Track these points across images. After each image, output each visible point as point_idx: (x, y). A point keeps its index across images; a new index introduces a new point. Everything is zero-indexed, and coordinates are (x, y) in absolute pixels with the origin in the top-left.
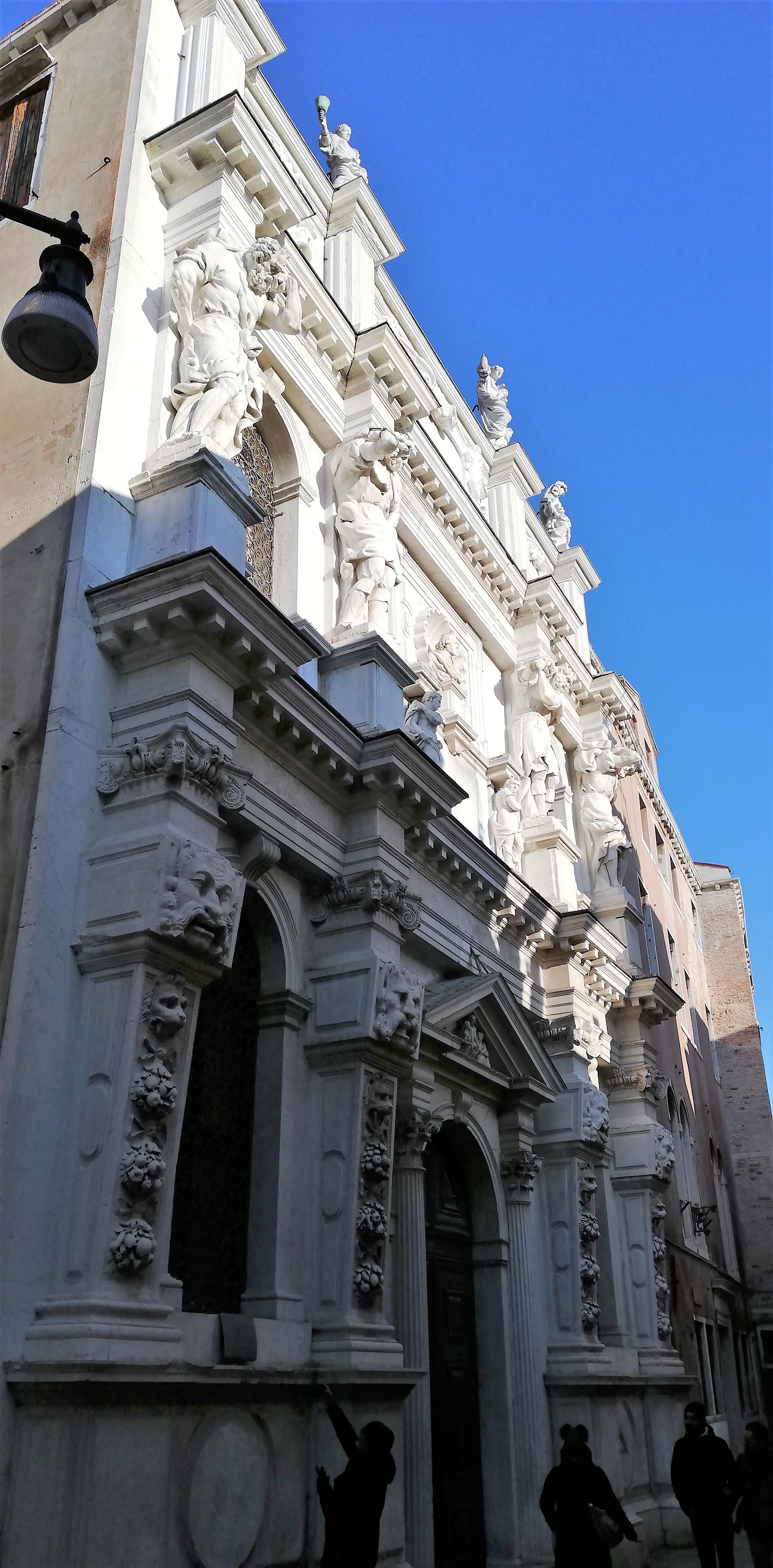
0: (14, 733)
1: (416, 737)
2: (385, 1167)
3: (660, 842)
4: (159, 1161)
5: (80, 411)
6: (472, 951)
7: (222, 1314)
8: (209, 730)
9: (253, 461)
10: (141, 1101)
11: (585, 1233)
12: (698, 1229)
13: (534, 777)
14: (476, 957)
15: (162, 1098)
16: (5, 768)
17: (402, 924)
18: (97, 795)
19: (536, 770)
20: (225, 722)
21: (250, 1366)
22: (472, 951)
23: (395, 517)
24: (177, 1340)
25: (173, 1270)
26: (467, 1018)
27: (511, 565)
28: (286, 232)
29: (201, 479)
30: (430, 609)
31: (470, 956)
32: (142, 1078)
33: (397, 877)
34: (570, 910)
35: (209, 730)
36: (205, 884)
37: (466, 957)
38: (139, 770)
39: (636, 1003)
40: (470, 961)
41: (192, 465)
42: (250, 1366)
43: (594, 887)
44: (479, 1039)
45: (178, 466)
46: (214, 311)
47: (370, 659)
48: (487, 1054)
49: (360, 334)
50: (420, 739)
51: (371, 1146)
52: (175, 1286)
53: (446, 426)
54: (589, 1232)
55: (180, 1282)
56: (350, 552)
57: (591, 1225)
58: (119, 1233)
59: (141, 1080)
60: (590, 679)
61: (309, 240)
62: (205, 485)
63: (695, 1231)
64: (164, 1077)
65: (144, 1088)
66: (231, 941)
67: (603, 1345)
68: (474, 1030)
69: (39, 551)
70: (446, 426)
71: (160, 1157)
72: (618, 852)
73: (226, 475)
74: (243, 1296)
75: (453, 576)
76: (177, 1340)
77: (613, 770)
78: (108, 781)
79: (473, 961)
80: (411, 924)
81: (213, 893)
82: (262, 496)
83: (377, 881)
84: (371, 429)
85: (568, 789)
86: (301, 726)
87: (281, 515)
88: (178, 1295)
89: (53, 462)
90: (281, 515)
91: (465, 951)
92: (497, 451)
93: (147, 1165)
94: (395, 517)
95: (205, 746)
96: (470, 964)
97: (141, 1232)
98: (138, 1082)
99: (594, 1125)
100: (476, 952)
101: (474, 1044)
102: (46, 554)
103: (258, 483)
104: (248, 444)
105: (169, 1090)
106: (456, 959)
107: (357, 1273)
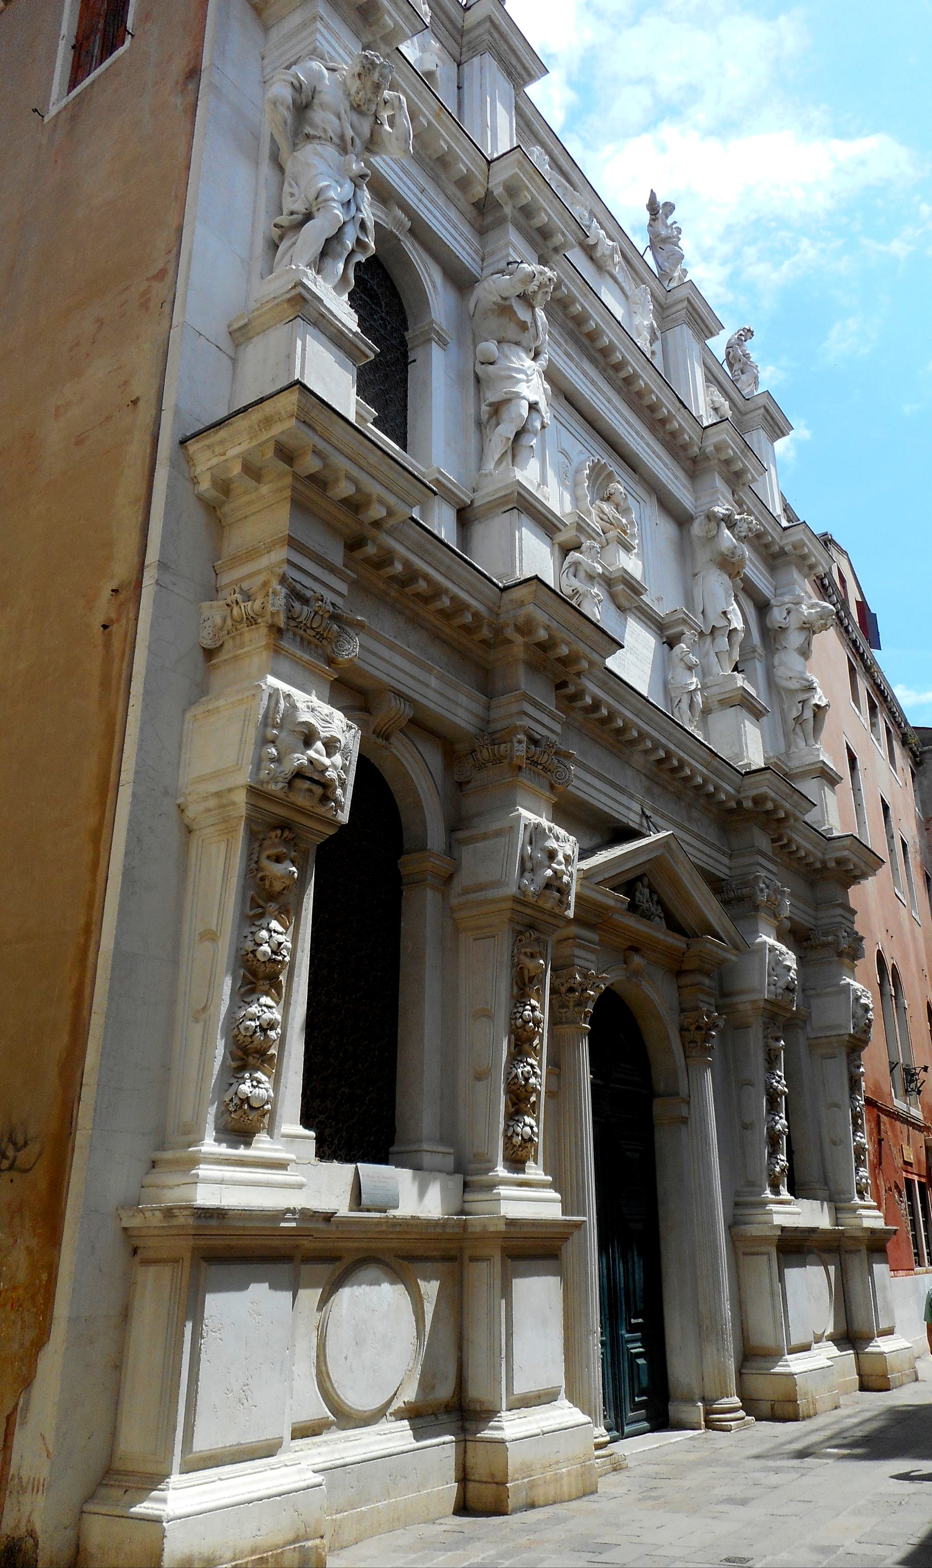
0: (113, 591)
1: (573, 591)
2: (537, 1023)
3: (873, 708)
4: (273, 1013)
5: (174, 251)
6: (643, 812)
7: (359, 1164)
8: (315, 579)
9: (381, 304)
10: (250, 955)
11: (771, 1090)
12: (910, 1090)
13: (717, 633)
14: (648, 817)
15: (273, 952)
16: (105, 627)
17: (553, 782)
18: (201, 651)
19: (717, 626)
20: (331, 569)
21: (392, 1213)
22: (643, 812)
23: (543, 361)
24: (300, 1186)
25: (307, 1120)
26: (640, 878)
27: (682, 409)
28: (397, 49)
29: (300, 314)
30: (592, 458)
31: (641, 817)
32: (252, 933)
33: (545, 732)
34: (753, 768)
35: (315, 579)
36: (308, 737)
37: (637, 819)
38: (241, 622)
39: (832, 864)
40: (641, 822)
41: (289, 300)
42: (392, 1213)
43: (790, 748)
44: (652, 900)
45: (276, 302)
46: (315, 137)
47: (511, 506)
48: (662, 915)
49: (493, 161)
50: (578, 592)
51: (521, 1003)
52: (308, 1138)
53: (609, 265)
54: (775, 1089)
55: (312, 1134)
56: (492, 396)
57: (778, 1082)
58: (231, 1084)
59: (250, 935)
60: (779, 530)
61: (437, 66)
62: (304, 320)
63: (906, 1091)
64: (275, 931)
65: (253, 942)
66: (345, 797)
67: (793, 1198)
68: (647, 891)
69: (135, 402)
70: (609, 265)
71: (274, 1010)
72: (814, 710)
73: (328, 310)
74: (391, 1149)
75: (617, 423)
76: (300, 1186)
77: (807, 626)
78: (211, 636)
79: (644, 821)
80: (563, 781)
81: (319, 745)
82: (393, 342)
83: (521, 737)
84: (508, 264)
85: (760, 650)
86: (426, 578)
87: (414, 361)
88: (312, 1146)
89: (147, 309)
90: (414, 361)
91: (636, 813)
92: (669, 291)
93: (259, 1018)
94: (543, 361)
95: (309, 594)
96: (641, 825)
97: (255, 1083)
98: (246, 937)
99: (779, 984)
100: (648, 813)
101: (645, 905)
102: (141, 404)
103: (388, 328)
104: (376, 288)
105: (280, 944)
106: (625, 820)
107: (509, 1126)
